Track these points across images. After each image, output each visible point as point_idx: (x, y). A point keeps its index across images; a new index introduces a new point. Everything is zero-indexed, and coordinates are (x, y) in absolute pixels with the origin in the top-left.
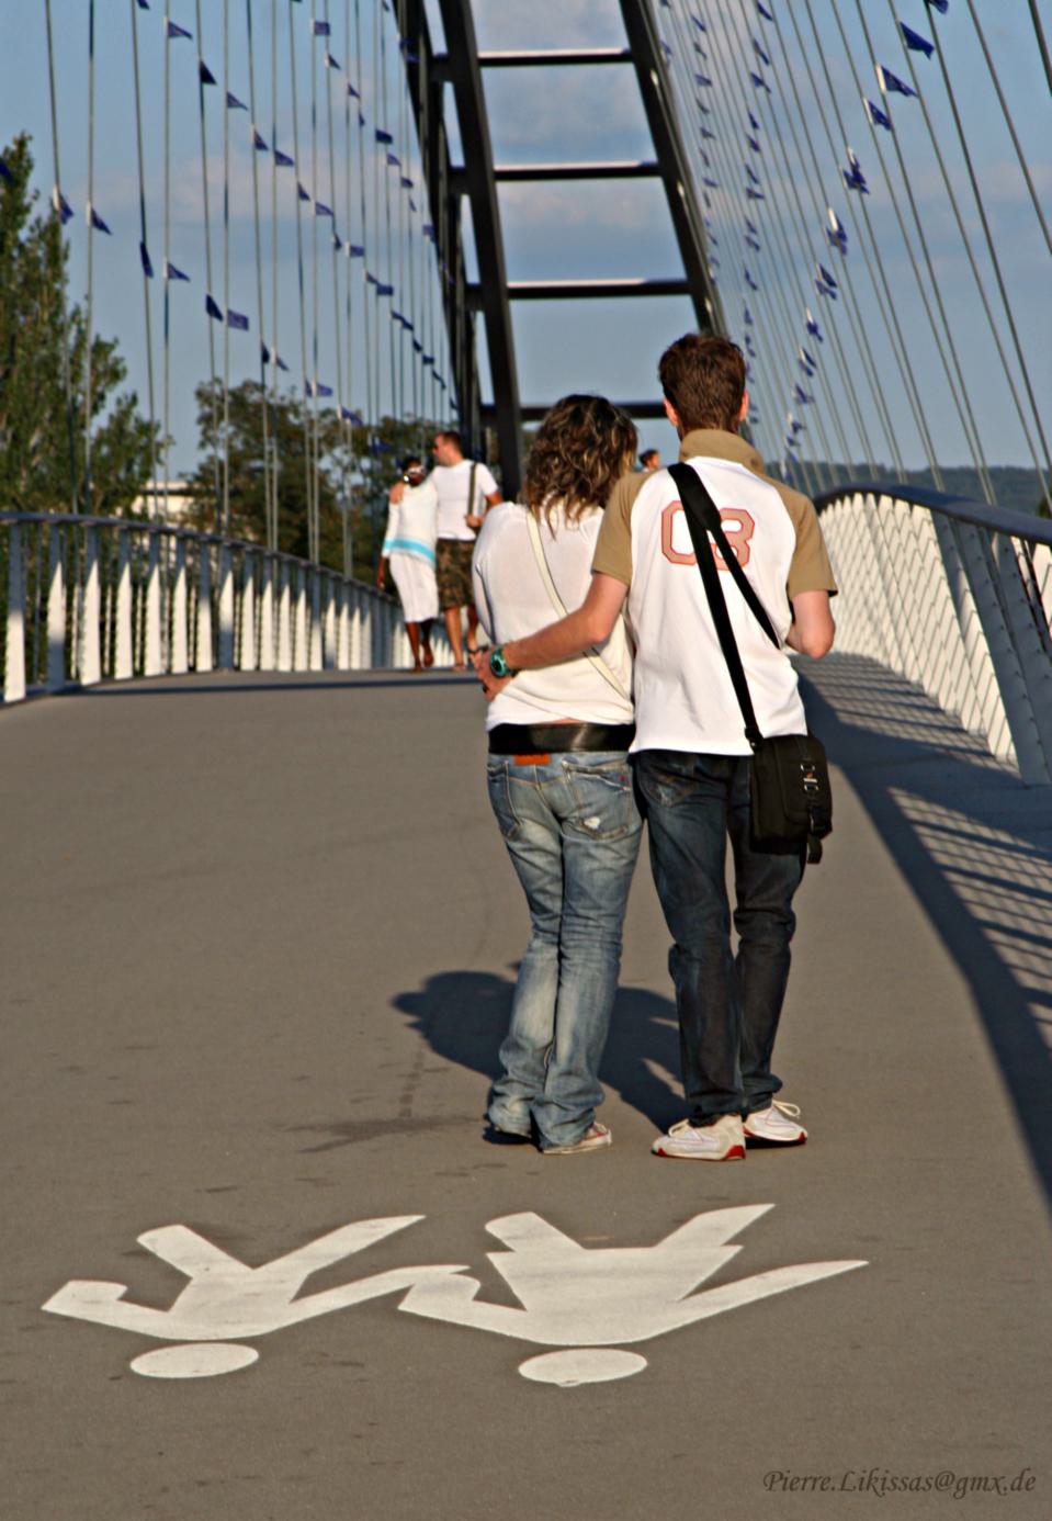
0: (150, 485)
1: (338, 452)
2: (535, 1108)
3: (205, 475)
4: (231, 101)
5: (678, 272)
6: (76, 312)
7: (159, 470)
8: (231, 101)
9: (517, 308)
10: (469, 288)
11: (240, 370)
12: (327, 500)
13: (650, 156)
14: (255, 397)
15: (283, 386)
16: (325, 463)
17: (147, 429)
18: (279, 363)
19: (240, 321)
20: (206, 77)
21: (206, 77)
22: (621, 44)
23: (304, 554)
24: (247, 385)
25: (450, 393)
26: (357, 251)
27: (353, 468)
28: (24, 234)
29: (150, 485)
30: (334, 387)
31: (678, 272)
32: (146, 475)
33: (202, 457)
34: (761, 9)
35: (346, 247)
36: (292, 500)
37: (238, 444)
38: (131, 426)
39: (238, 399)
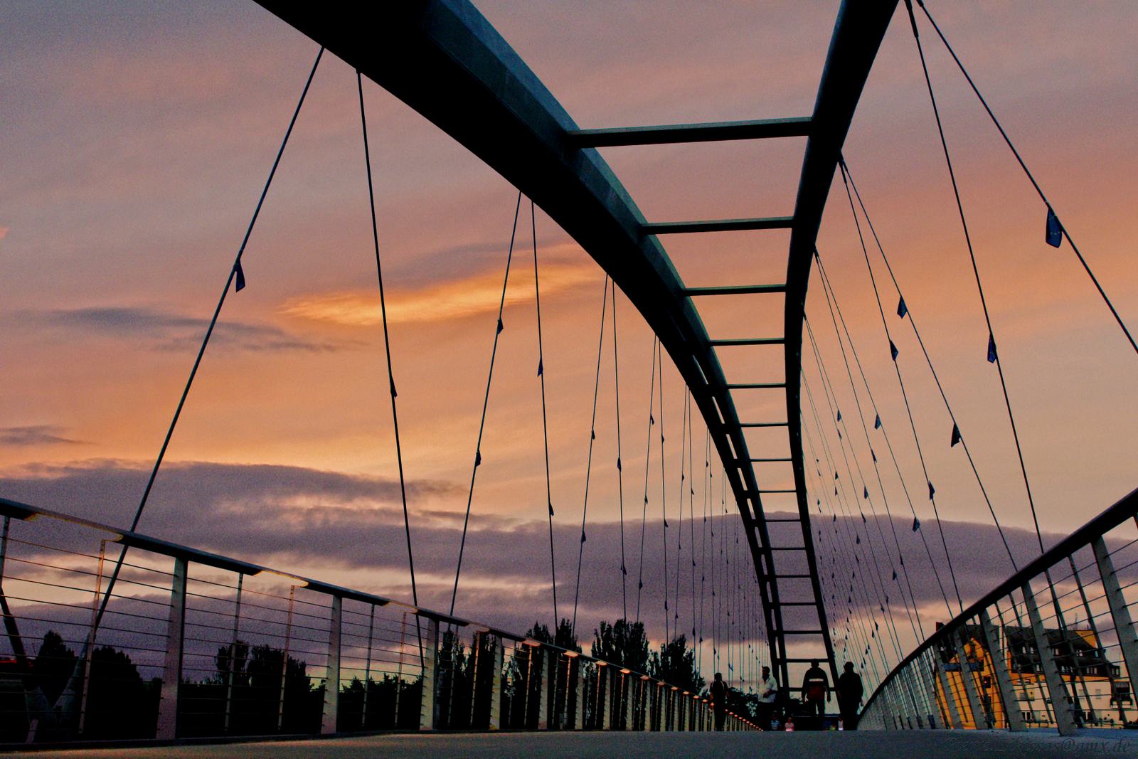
16: (748, 705)
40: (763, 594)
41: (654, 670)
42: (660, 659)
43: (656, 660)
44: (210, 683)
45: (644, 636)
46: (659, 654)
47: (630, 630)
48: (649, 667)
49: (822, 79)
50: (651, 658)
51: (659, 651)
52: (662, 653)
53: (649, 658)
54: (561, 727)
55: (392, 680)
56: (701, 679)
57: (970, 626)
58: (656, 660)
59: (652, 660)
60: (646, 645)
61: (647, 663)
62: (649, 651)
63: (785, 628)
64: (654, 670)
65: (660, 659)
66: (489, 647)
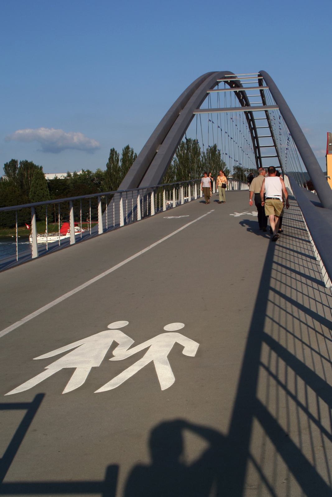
0: (229, 175)
1: (246, 172)
2: (276, 217)
3: (234, 174)
4: (236, 143)
5: (279, 166)
6: (222, 160)
7: (229, 174)
8: (236, 143)
9: (262, 159)
10: (257, 157)
11: (237, 164)
12: (245, 176)
13: (277, 155)
14: (238, 167)
15: (241, 166)
16: (245, 173)
17: (228, 170)
18: (232, 158)
19: (237, 161)
20: (234, 141)
21: (234, 141)
22: (273, 145)
23: (243, 180)
24: (238, 166)
25: (256, 166)
26: (247, 154)
27: (247, 173)
28: (217, 153)
29: (229, 175)
30: (238, 161)
31: (279, 166)
32: (228, 174)
33: (234, 173)
34: (271, 490)
35: (239, 147)
36: (242, 177)
37: (237, 171)
38: (227, 170)
39: (237, 167)
40: (252, 133)
41: (204, 160)
42: (206, 155)
43: (204, 156)
44: (85, 172)
45: (199, 145)
46: (206, 153)
47: (192, 143)
48: (201, 159)
49: (267, 74)
50: (202, 155)
51: (206, 152)
52: (207, 153)
53: (201, 155)
54: (175, 185)
55: (86, 172)
56: (224, 163)
57: (206, 456)
58: (204, 156)
59: (203, 155)
60: (200, 149)
61: (200, 157)
62: (201, 152)
63: (274, 147)
64: (204, 160)
65: (206, 155)
66: (130, 154)
